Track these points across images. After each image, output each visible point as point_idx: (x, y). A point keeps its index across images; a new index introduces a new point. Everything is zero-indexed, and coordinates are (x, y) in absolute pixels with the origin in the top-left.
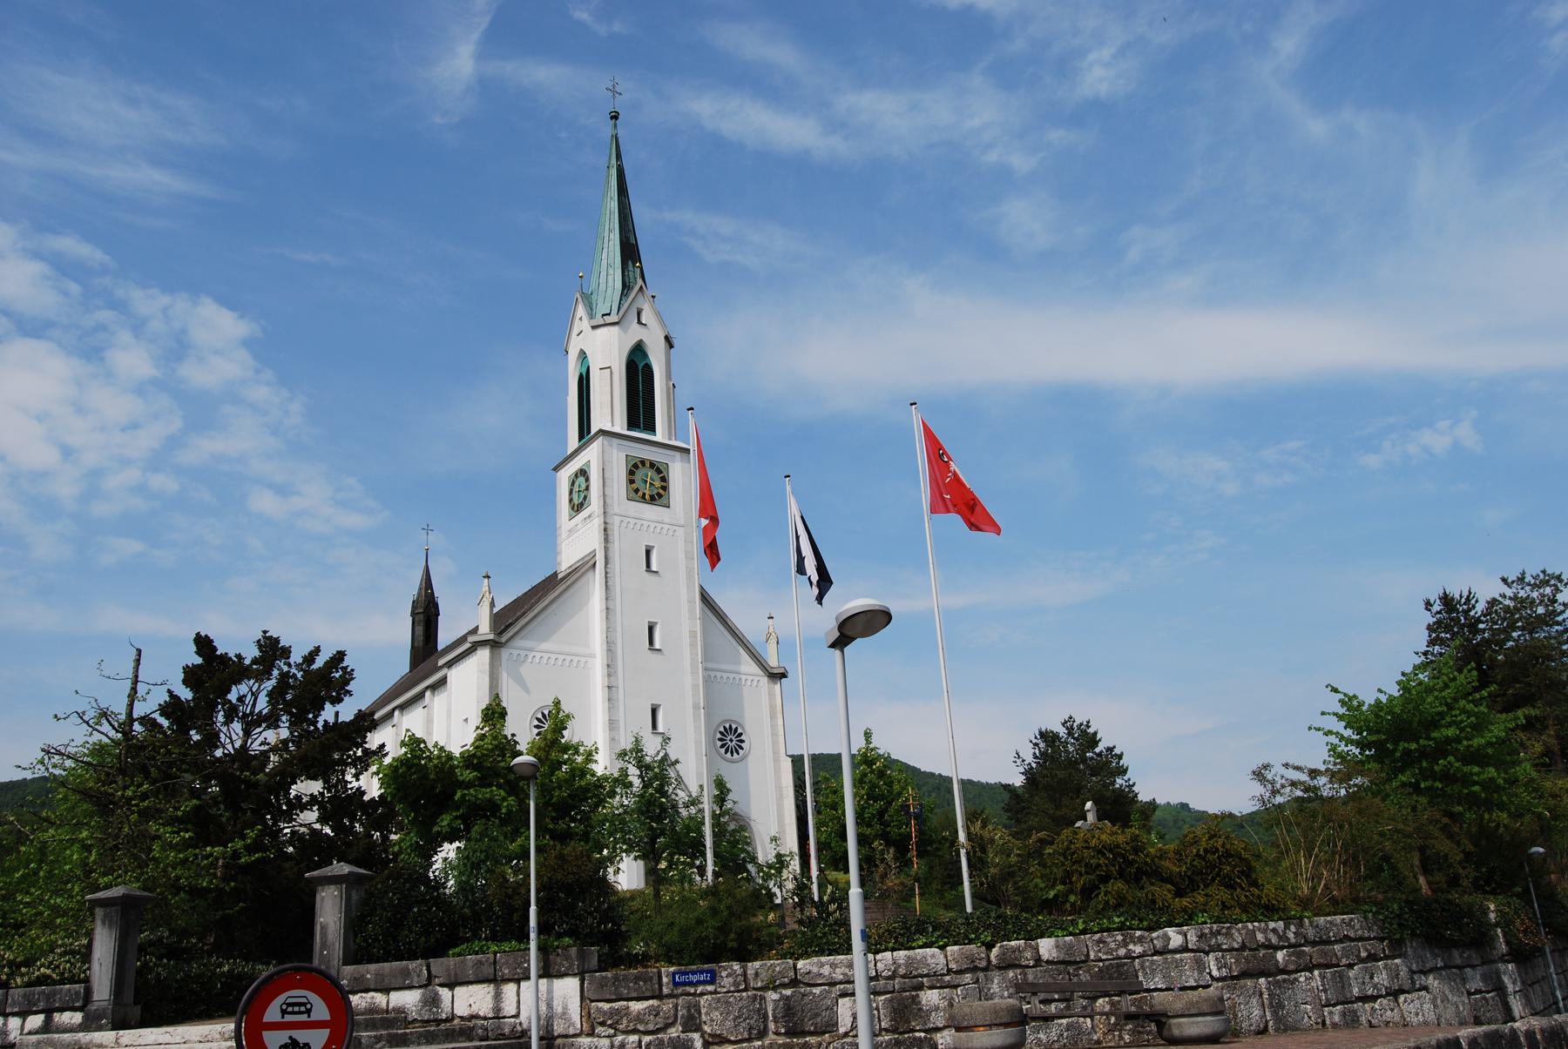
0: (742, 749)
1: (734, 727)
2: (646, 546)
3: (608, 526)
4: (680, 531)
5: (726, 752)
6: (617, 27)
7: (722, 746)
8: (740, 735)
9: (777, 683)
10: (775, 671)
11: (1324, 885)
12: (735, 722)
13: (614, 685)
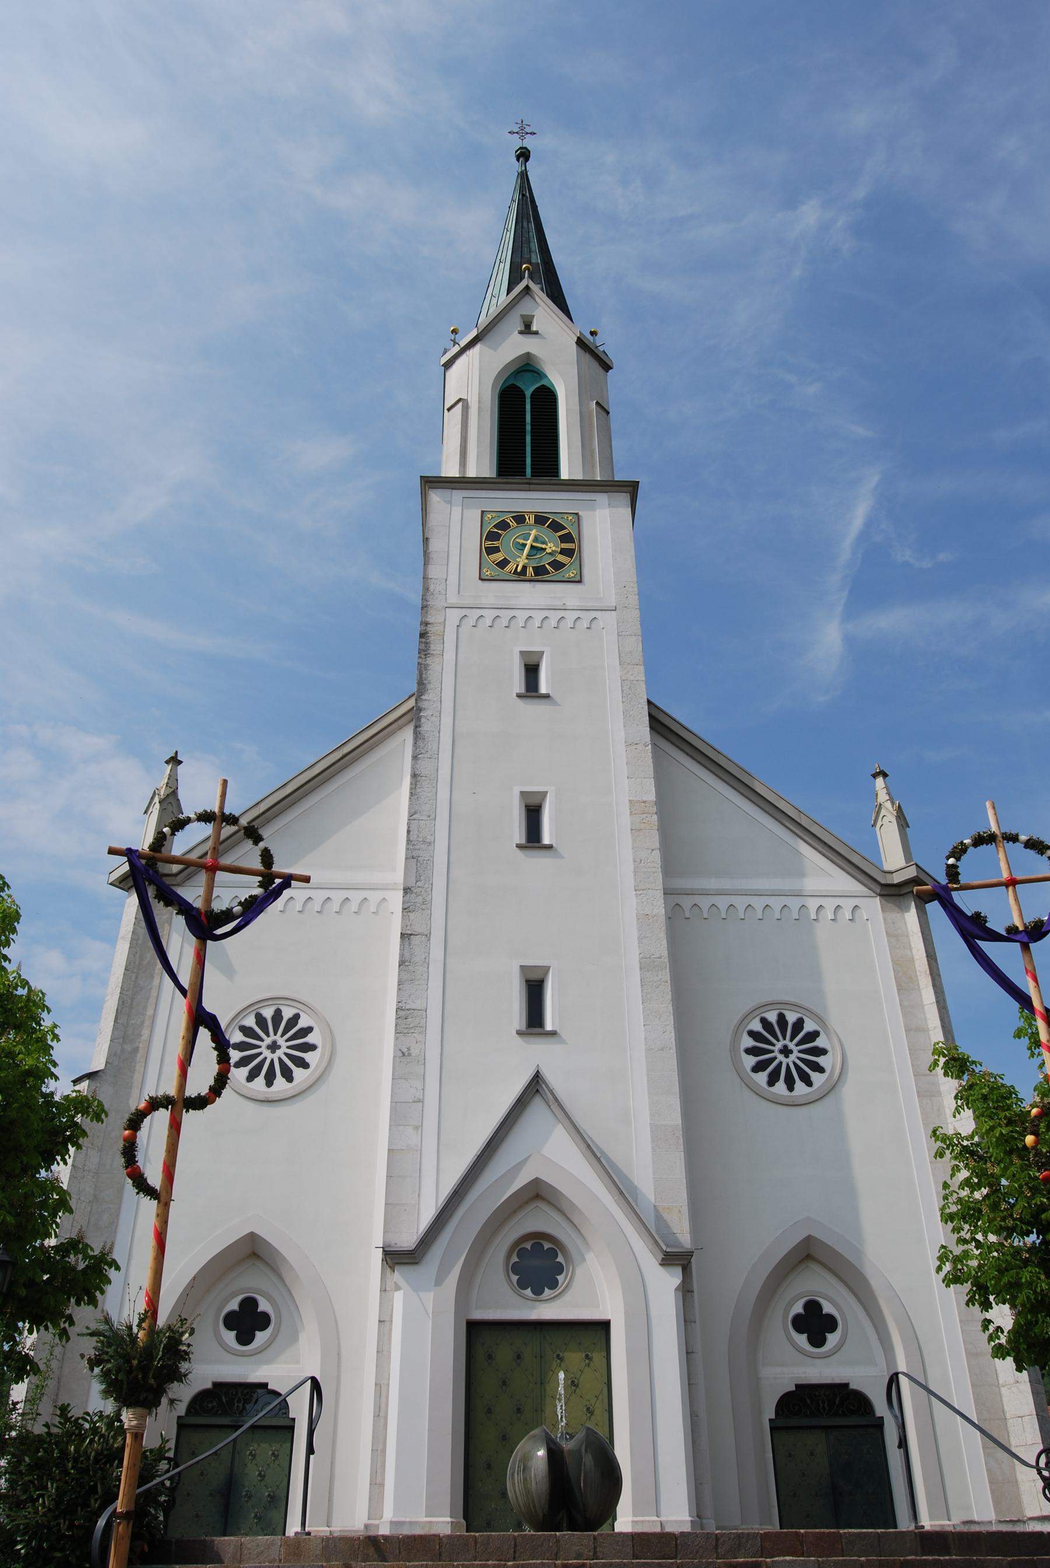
0: (820, 1069)
1: (772, 1017)
2: (523, 653)
3: (429, 628)
4: (609, 620)
5: (790, 1085)
6: (943, 557)
7: (772, 1080)
8: (813, 1035)
9: (908, 909)
10: (897, 879)
11: (532, 1560)
12: (794, 1006)
13: (418, 929)
